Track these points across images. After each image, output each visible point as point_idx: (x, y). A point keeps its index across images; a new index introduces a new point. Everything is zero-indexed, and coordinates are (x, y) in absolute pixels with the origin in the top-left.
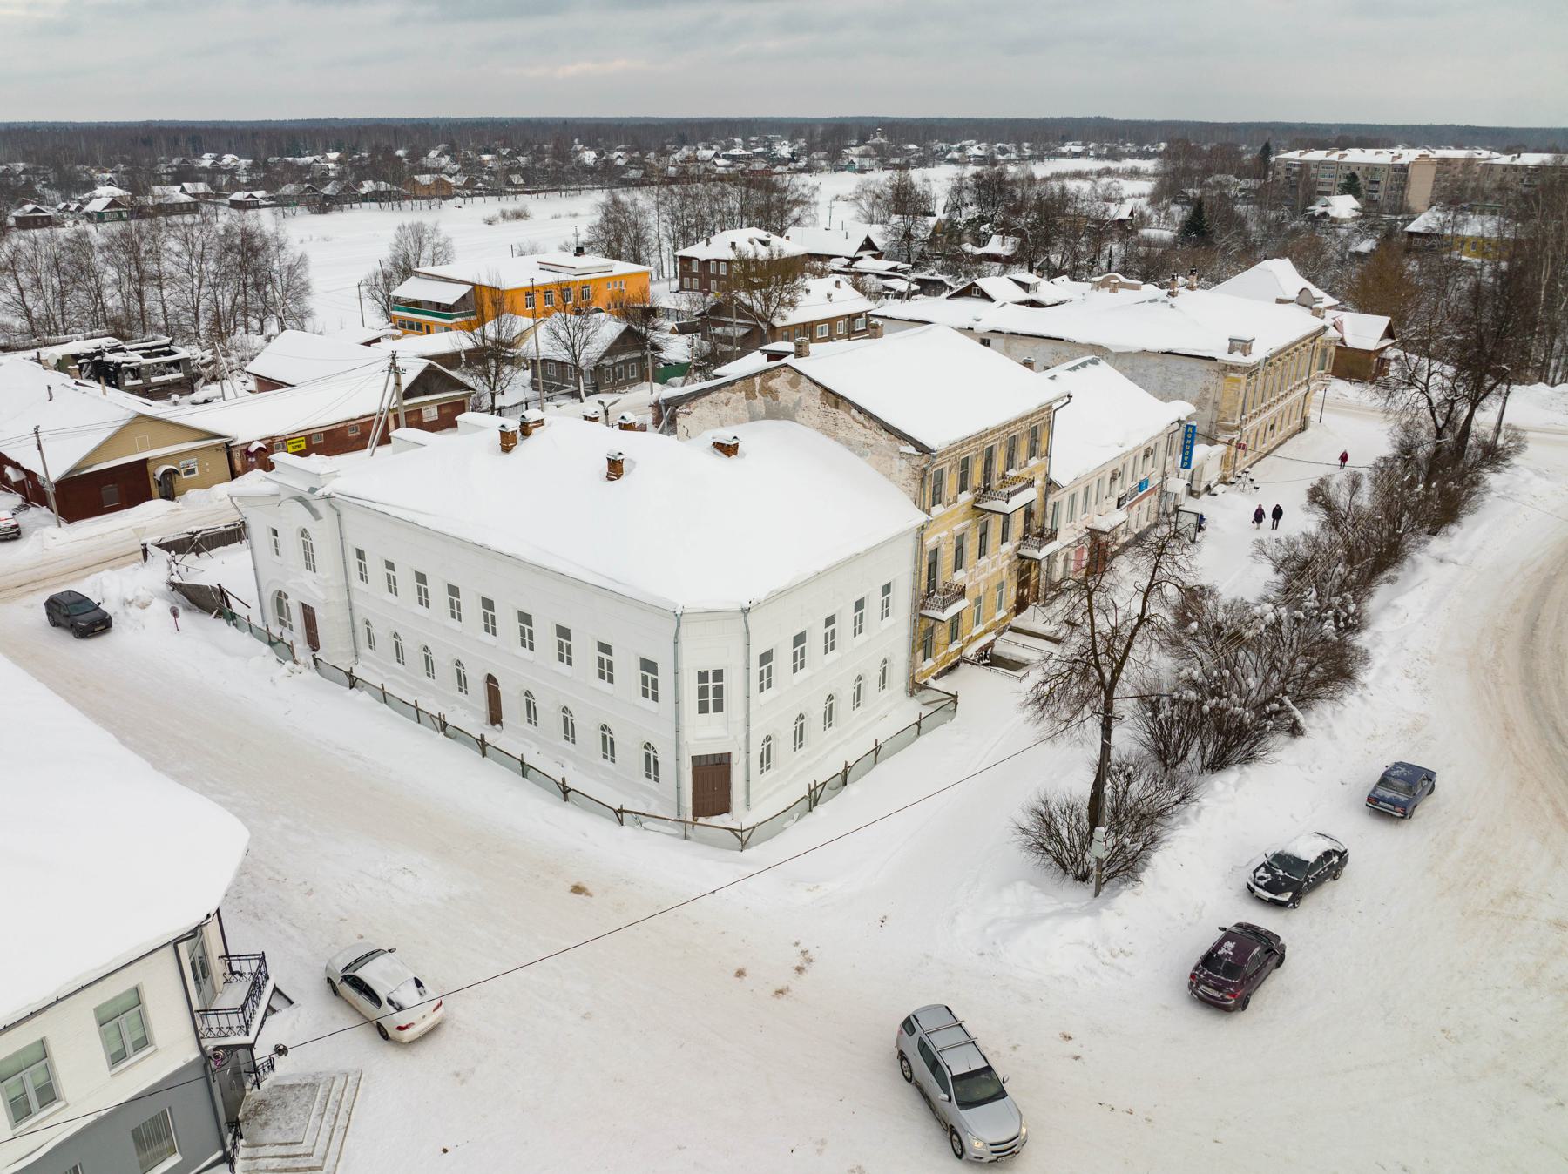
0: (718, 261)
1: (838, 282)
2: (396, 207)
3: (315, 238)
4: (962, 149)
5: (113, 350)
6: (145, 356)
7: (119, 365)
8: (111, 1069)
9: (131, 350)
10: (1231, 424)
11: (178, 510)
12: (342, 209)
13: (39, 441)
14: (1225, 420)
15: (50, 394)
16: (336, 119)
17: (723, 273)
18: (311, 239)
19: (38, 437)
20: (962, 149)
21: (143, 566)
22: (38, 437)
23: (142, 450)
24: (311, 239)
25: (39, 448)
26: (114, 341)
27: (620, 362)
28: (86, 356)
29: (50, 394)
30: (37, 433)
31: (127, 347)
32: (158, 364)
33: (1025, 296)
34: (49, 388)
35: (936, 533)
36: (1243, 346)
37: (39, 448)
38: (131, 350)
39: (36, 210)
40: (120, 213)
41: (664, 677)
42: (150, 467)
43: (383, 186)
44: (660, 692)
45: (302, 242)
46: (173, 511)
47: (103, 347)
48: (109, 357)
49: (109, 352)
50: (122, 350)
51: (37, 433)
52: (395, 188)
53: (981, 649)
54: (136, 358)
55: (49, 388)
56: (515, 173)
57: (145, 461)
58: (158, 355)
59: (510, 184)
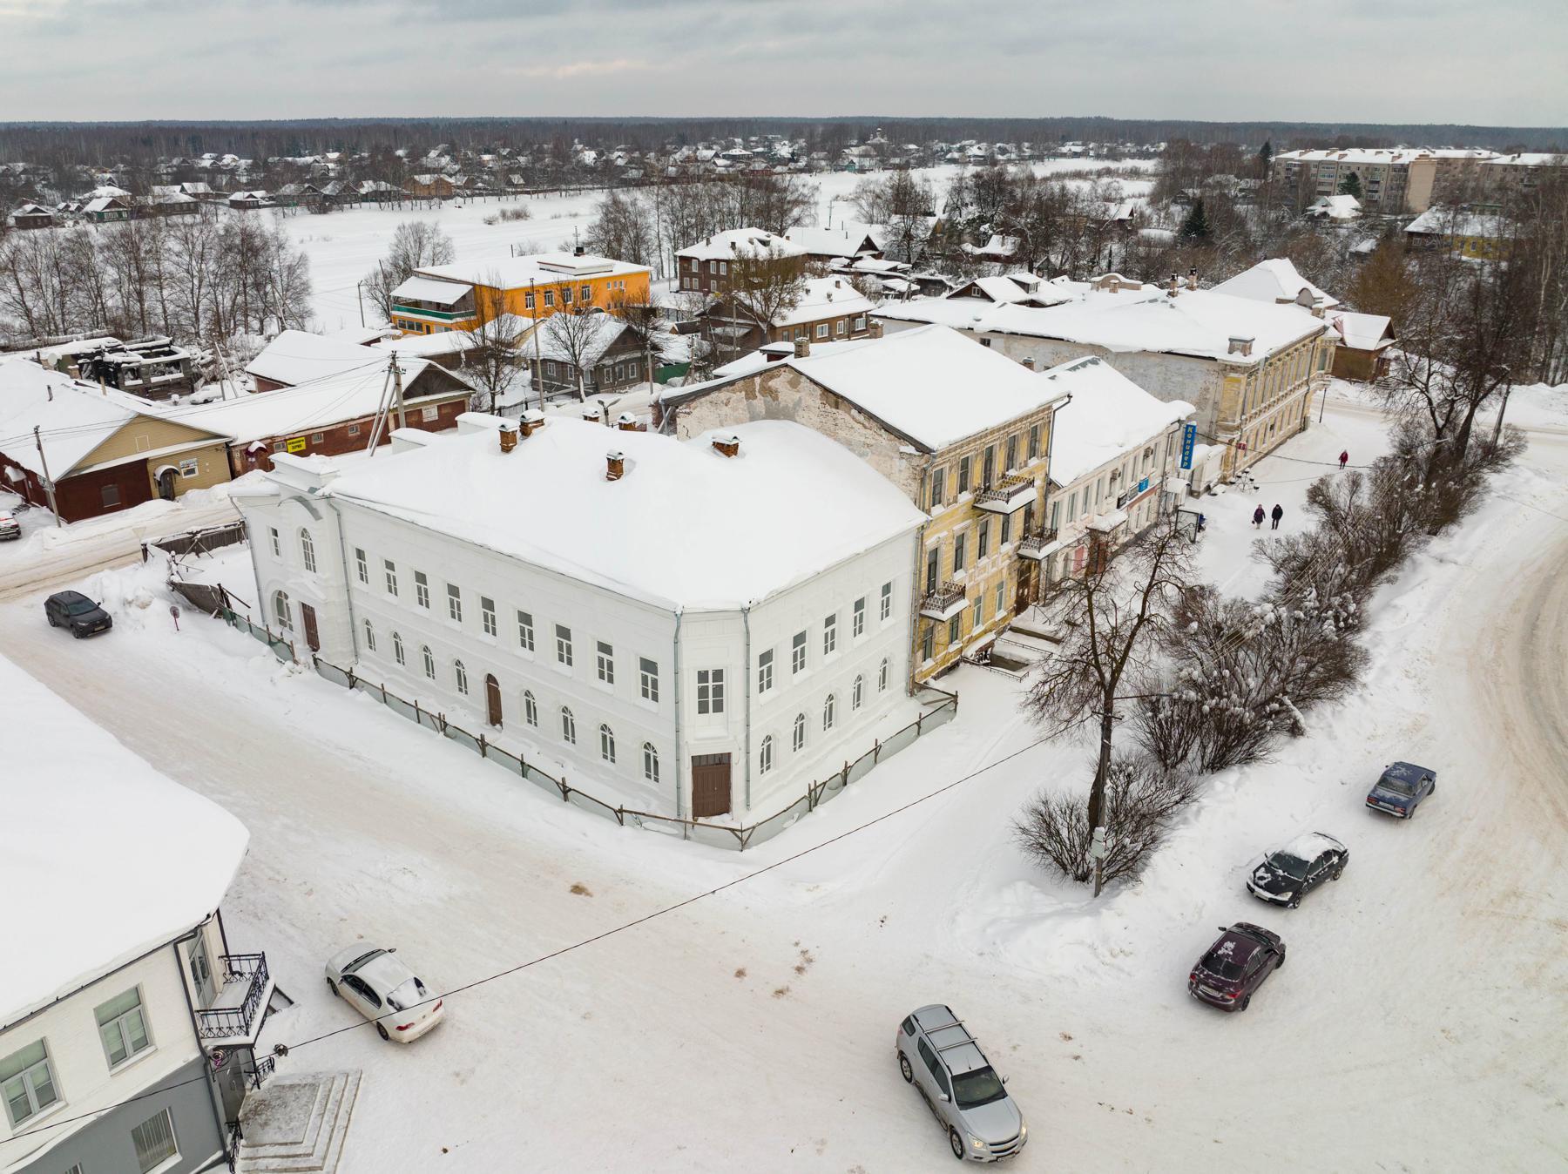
0: (718, 261)
1: (838, 282)
2: (396, 207)
3: (315, 238)
4: (962, 149)
5: (113, 350)
6: (145, 356)
7: (119, 365)
8: (111, 1069)
9: (131, 350)
10: (1231, 424)
11: (178, 510)
12: (342, 209)
13: (39, 441)
14: (1225, 420)
15: (50, 394)
16: (336, 119)
17: (723, 273)
18: (311, 239)
19: (38, 437)
20: (962, 149)
21: (143, 566)
22: (38, 437)
23: (142, 450)
24: (311, 239)
25: (39, 448)
26: (114, 341)
27: (620, 362)
28: (86, 356)
29: (50, 394)
30: (37, 433)
31: (127, 347)
32: (158, 364)
33: (1025, 296)
34: (49, 388)
35: (936, 533)
36: (1243, 346)
37: (39, 448)
38: (131, 350)
39: (36, 210)
40: (120, 213)
41: (664, 677)
42: (150, 467)
43: (383, 186)
44: (660, 692)
45: (302, 242)
46: (173, 511)
47: (103, 347)
48: (109, 357)
49: (109, 352)
50: (122, 350)
51: (37, 433)
52: (395, 188)
53: (981, 649)
54: (136, 358)
55: (49, 388)
56: (515, 173)
57: (145, 461)
58: (158, 355)
59: (510, 184)
